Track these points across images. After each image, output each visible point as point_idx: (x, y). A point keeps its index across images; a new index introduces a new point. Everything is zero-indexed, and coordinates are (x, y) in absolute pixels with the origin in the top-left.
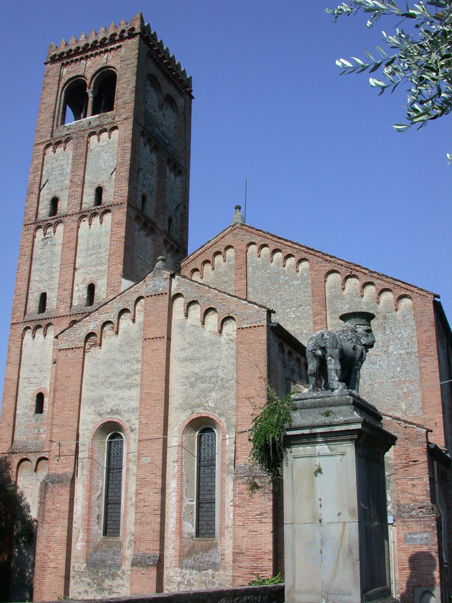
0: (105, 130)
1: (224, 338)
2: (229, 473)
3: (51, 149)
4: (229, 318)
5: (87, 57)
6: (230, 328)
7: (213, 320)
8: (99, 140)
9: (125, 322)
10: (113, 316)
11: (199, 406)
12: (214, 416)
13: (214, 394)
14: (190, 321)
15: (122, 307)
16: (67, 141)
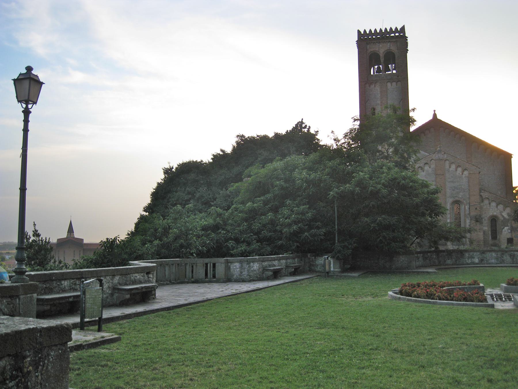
0: (394, 81)
1: (464, 176)
2: (467, 217)
3: (367, 85)
4: (466, 169)
5: (379, 42)
6: (466, 173)
7: (460, 170)
8: (391, 85)
9: (426, 168)
10: (421, 165)
11: (456, 197)
12: (462, 200)
13: (461, 193)
14: (451, 169)
15: (425, 162)
16: (376, 83)
